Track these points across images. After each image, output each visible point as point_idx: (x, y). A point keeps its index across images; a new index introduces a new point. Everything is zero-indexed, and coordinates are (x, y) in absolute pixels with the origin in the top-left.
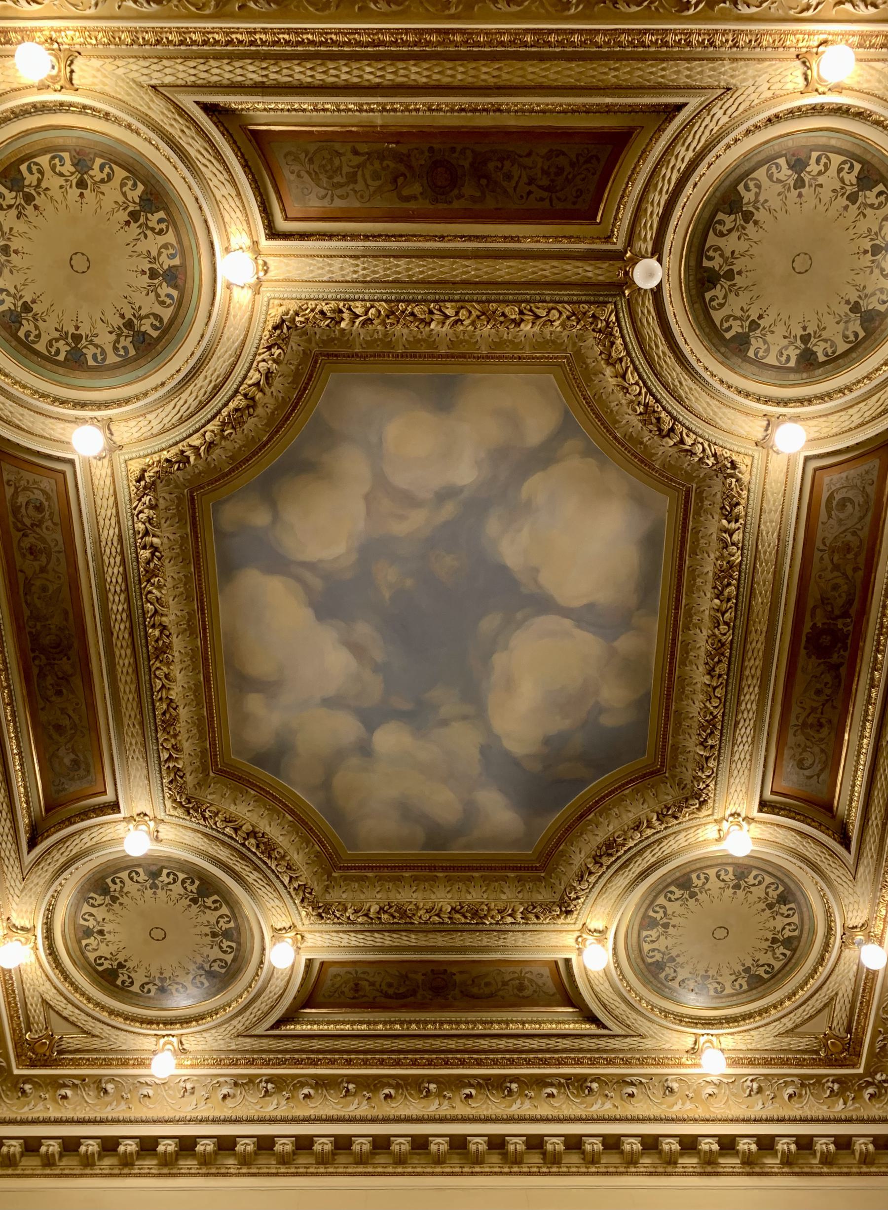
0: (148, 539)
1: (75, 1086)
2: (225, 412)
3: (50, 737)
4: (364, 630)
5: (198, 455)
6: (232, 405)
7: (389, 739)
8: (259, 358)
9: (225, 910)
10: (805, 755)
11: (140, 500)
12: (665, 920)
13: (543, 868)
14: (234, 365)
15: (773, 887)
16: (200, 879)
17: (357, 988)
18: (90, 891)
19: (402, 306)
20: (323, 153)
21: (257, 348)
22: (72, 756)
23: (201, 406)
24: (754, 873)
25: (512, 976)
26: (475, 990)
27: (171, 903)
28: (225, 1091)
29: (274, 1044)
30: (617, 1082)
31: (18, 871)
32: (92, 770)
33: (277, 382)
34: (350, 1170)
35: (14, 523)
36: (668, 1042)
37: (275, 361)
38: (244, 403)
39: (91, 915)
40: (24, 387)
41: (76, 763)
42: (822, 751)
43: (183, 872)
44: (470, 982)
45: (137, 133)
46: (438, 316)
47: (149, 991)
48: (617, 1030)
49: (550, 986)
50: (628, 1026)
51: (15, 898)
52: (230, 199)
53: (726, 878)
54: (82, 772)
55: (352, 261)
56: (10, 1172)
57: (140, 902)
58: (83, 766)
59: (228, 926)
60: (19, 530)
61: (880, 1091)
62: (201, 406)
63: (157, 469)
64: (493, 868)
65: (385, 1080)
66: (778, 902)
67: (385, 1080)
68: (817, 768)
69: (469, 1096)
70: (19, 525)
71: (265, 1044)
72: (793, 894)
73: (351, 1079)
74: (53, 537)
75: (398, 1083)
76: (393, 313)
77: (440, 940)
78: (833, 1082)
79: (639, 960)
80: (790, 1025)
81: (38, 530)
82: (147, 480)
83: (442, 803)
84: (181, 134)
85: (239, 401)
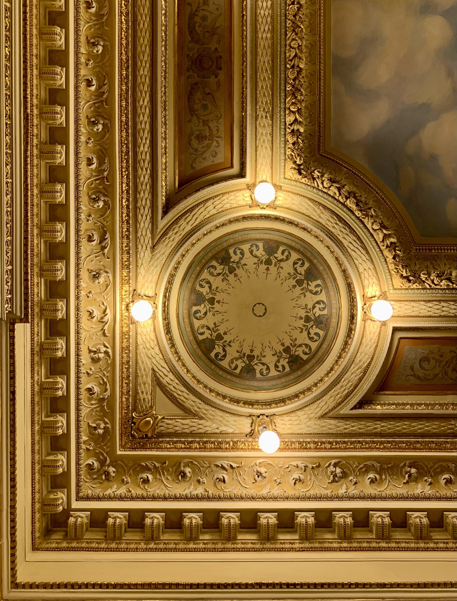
2: (358, 213)
5: (389, 236)
8: (321, 186)
10: (433, 362)
11: (424, 282)
12: (274, 261)
14: (325, 207)
15: (307, 350)
20: (188, 141)
23: (353, 231)
24: (321, 333)
25: (214, 130)
26: (198, 95)
29: (355, 427)
30: (103, 226)
36: (147, 271)
37: (322, 176)
40: (332, 369)
42: (436, 375)
44: (207, 91)
45: (179, 263)
46: (296, 61)
48: (162, 224)
49: (200, 165)
50: (165, 234)
53: (316, 310)
55: (259, 119)
61: (94, 474)
62: (353, 231)
63: (400, 267)
66: (291, 356)
68: (420, 373)
69: (89, 83)
72: (298, 369)
78: (104, 428)
79: (232, 241)
80: (165, 380)
82: (409, 274)
83: (378, 72)
84: (178, 234)
85: (350, 203)
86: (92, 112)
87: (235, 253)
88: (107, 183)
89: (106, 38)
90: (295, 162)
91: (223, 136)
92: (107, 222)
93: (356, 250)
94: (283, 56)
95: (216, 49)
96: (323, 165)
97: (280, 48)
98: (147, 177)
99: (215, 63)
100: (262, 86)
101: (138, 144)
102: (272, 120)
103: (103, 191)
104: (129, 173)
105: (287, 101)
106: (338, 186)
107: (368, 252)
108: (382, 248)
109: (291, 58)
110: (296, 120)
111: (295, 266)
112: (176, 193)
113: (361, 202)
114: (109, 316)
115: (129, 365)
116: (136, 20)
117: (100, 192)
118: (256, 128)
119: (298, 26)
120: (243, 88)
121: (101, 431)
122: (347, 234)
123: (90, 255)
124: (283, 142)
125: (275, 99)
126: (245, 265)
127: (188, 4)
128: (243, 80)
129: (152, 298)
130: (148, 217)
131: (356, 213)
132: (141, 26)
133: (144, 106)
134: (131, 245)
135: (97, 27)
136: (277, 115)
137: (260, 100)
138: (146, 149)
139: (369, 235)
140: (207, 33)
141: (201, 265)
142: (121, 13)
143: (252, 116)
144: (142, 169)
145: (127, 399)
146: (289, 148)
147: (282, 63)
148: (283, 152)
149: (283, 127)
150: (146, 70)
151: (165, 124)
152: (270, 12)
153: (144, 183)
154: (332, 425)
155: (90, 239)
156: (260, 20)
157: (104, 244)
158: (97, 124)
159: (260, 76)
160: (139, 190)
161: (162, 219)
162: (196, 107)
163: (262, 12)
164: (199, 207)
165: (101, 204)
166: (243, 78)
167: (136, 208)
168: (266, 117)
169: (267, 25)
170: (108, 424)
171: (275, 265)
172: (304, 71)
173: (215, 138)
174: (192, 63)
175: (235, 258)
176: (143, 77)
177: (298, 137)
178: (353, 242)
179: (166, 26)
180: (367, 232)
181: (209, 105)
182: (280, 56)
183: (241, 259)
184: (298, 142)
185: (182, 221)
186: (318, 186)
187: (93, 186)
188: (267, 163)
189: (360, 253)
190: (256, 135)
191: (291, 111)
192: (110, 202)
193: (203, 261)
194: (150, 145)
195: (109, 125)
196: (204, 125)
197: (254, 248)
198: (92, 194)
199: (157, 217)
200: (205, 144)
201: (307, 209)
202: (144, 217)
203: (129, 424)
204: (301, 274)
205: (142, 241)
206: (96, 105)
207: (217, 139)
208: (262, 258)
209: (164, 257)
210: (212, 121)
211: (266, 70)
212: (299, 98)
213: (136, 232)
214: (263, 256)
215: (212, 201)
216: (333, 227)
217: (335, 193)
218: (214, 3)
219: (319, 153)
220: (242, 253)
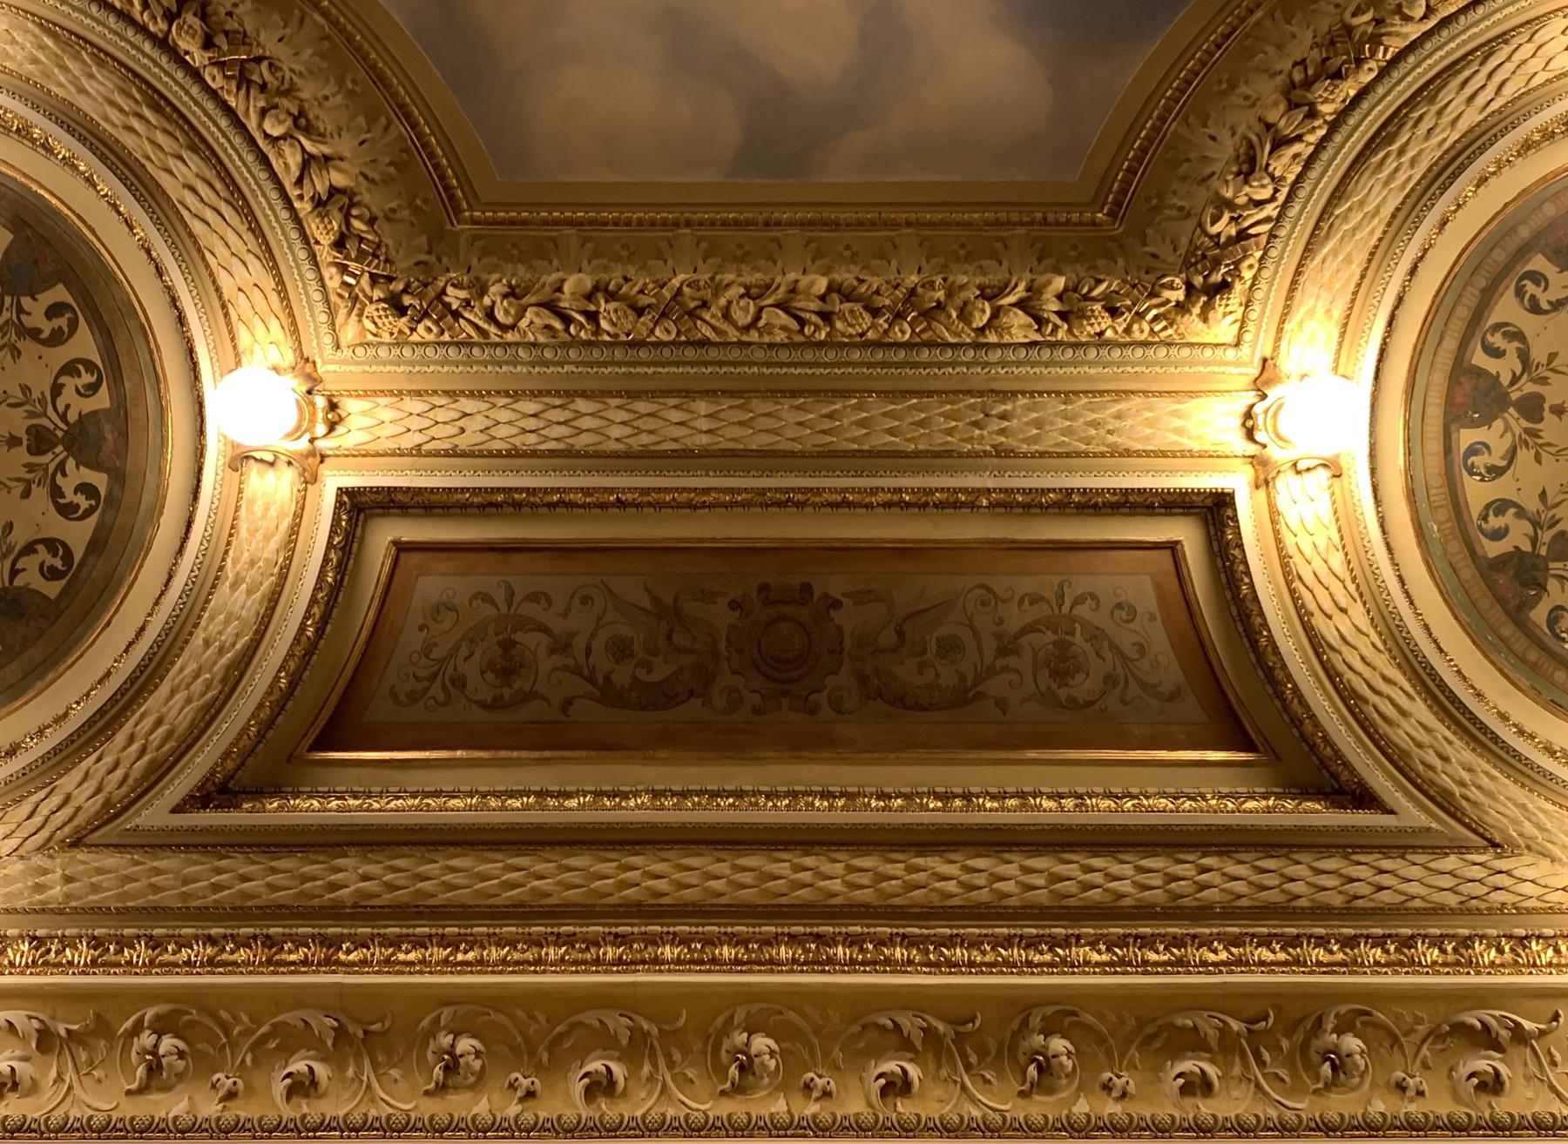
6: (1349, 89)
8: (1270, 210)
9: (84, 344)
11: (456, 315)
12: (1527, 387)
14: (1337, 195)
17: (508, 665)
19: (903, 333)
21: (1272, 236)
23: (1428, 91)
25: (1033, 613)
29: (201, 878)
30: (1435, 1035)
33: (1225, 150)
37: (1230, 205)
38: (1319, 91)
44: (887, 638)
46: (808, 305)
48: (1411, 813)
49: (1165, 664)
50: (1445, 802)
52: (1327, 605)
55: (1011, 442)
62: (1428, 91)
65: (590, 1018)
69: (897, 1087)
71: (177, 877)
73: (473, 1012)
76: (927, 314)
77: (790, 424)
79: (1455, 546)
84: (1449, 750)
86: (1000, 1073)
87: (1498, 535)
88: (1271, 1021)
89: (720, 1021)
90: (1182, 308)
91: (1056, 580)
92: (1418, 1021)
93: (1497, 79)
94: (784, 355)
95: (734, 605)
96: (1156, 210)
97: (751, 364)
98: (1233, 869)
99: (788, 610)
100: (891, 432)
101: (1109, 898)
102: (1014, 394)
103: (1299, 1037)
104: (1220, 937)
105: (951, 340)
106: (1268, 148)
109: (794, 325)
110: (1021, 304)
111: (1545, 306)
112: (1278, 759)
113: (1324, 60)
115: (110, 938)
116: (639, 905)
117: (1305, 1047)
118: (1042, 455)
119: (674, 298)
120: (603, 506)
122: (1440, 113)
123: (1553, 1088)
124: (1104, 352)
125: (932, 385)
126: (1543, 495)
127: (564, 711)
128: (576, 505)
130: (1386, 864)
131: (1366, 78)
132: (661, 885)
133: (965, 878)
134: (1494, 932)
135: (677, 1056)
136: (997, 378)
137: (939, 441)
138: (1127, 870)
139: (1445, 33)
140: (676, 639)
141: (1547, 665)
142: (211, 962)
143: (1001, 471)
144: (1203, 887)
146: (1128, 330)
147: (809, 356)
148: (1139, 352)
149: (1046, 354)
150: (827, 867)
152: (614, 402)
153: (1255, 878)
155: (1492, 1085)
156: (645, 439)
157: (1505, 1034)
158: (455, 1058)
159: (853, 440)
160: (1282, 898)
161: (1392, 812)
162: (948, 679)
163: (616, 432)
164: (1342, 667)
165: (1352, 1043)
166: (850, 505)
167: (1348, 912)
168: (1004, 416)
169: (665, 414)
170: (140, 1021)
171: (1543, 381)
172: (837, 277)
173: (1065, 609)
174: (785, 693)
175: (1519, 536)
177: (1086, 298)
178: (1469, 90)
179: (598, 794)
180: (1436, 40)
181: (943, 631)
182: (781, 365)
183: (1521, 513)
184: (1106, 297)
185: (1399, 737)
186: (1267, 220)
187: (1283, 1073)
188: (1176, 414)
189: (1510, 66)
190: (1068, 455)
191: (989, 325)
192: (1343, 1009)
193: (1533, 655)
194: (1112, 854)
195: (1049, 1010)
196: (1016, 652)
197: (1479, 461)
198: (1317, 1078)
199: (1385, 831)
200: (1087, 647)
201: (1348, 260)
202: (1385, 880)
204: (14, 573)
205: (1480, 890)
206: (973, 1059)
207: (1068, 603)
208: (1518, 431)
209: (1539, 805)
210: (1001, 621)
211: (830, 416)
212: (940, 294)
213: (1439, 911)
214: (1507, 428)
215: (1318, 621)
216: (1413, 162)
217: (1295, 156)
218: (565, 615)
219: (1138, 223)
220: (1500, 506)
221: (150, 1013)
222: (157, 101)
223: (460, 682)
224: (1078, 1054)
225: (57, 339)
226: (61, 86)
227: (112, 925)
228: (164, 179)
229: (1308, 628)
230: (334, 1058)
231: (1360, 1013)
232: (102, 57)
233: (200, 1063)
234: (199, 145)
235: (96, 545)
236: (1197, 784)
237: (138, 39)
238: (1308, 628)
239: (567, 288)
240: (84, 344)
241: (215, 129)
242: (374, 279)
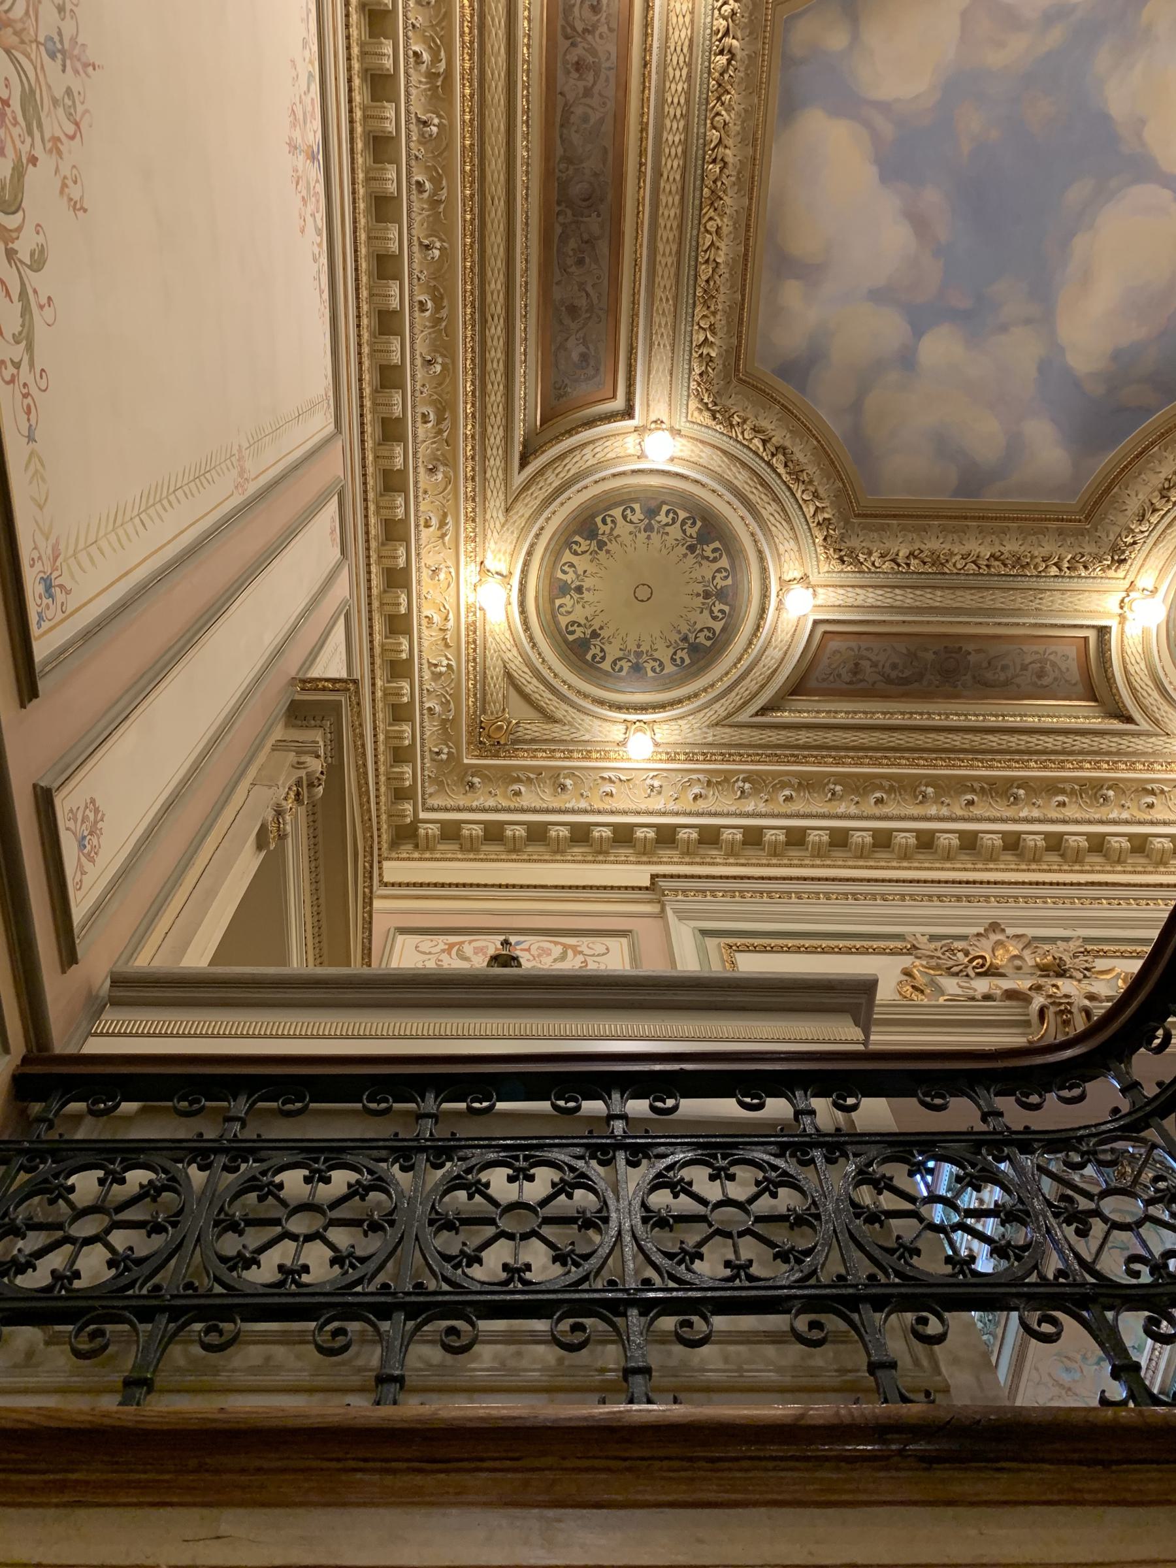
0: (728, 41)
1: (529, 779)
3: (561, 322)
4: (932, 197)
7: (940, 348)
11: (862, 563)
13: (1088, 518)
16: (703, 519)
17: (856, 670)
18: (575, 533)
22: (582, 349)
26: (989, 675)
27: (664, 552)
28: (696, 790)
29: (756, 736)
30: (1136, 791)
31: (502, 496)
32: (602, 369)
34: (850, 863)
35: (563, 27)
37: (1132, 531)
39: (572, 565)
41: (584, 357)
43: (685, 509)
44: (985, 664)
45: (542, 528)
47: (621, 669)
51: (495, 534)
54: (590, 371)
56: (472, 856)
57: (630, 549)
58: (592, 363)
59: (724, 583)
60: (567, 38)
64: (1033, 519)
65: (877, 781)
67: (877, 781)
69: (971, 803)
70: (569, 30)
71: (746, 735)
73: (840, 779)
74: (606, 47)
75: (892, 787)
77: (968, 599)
81: (589, 38)
83: (983, 434)
90: (1109, 567)
95: (934, 653)
96: (1104, 519)
107: (792, 529)
108: (812, 525)
114: (451, 624)
121: (444, 757)
129: (505, 577)
145: (475, 686)
151: (526, 339)
154: (726, 734)
162: (1002, 677)
172: (722, 266)
176: (495, 294)
203: (478, 727)
204: (696, 638)
218: (600, 94)
221: (741, 777)
222: (764, 483)
223: (839, 676)
224: (1026, 794)
225: (715, 560)
226: (728, 475)
227: (728, 752)
228: (763, 511)
229: (1125, 668)
230: (797, 790)
231: (1115, 785)
232: (744, 465)
233: (756, 791)
234: (777, 499)
235: (723, 629)
236: (1078, 714)
237: (760, 462)
238: (1125, 668)
239: (901, 554)
240: (617, 512)
241: (784, 495)
242: (835, 550)
